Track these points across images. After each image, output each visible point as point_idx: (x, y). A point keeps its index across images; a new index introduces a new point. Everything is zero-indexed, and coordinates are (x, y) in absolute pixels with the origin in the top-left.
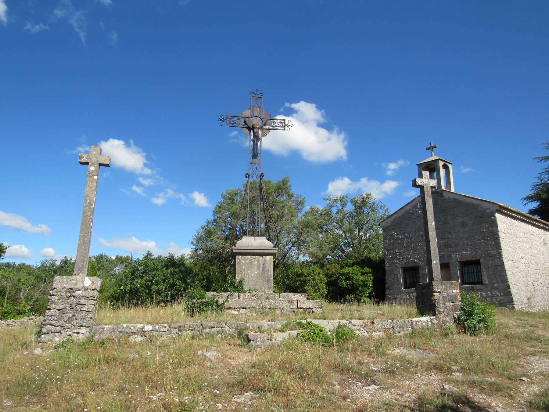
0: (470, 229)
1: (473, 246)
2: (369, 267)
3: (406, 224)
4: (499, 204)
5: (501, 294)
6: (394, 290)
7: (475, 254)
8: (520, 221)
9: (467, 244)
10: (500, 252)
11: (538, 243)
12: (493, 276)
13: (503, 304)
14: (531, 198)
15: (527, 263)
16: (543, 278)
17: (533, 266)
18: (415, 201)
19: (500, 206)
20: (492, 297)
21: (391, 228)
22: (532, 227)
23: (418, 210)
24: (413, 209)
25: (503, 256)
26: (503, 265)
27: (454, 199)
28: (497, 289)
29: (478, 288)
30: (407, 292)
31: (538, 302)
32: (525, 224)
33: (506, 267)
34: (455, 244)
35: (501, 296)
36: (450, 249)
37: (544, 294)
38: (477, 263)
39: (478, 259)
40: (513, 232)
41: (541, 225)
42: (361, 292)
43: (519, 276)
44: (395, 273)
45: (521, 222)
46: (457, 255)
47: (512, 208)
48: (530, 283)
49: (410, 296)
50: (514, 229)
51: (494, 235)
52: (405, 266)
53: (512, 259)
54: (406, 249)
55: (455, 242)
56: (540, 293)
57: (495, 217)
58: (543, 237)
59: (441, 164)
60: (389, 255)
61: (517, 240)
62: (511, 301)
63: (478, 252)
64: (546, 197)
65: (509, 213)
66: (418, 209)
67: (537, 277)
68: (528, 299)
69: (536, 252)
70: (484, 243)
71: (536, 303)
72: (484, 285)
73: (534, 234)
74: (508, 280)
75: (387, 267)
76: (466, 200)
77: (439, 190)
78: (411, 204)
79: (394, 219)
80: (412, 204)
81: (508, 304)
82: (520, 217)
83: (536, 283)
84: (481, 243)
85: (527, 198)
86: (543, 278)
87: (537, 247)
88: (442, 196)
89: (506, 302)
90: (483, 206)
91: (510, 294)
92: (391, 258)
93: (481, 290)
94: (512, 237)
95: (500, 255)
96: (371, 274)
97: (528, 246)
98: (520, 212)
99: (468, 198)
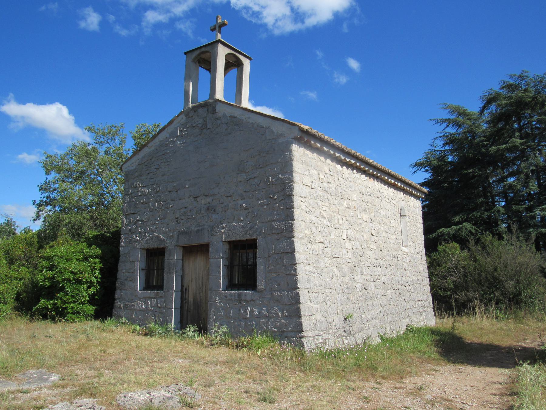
0: (249, 177)
1: (250, 210)
2: (94, 245)
3: (157, 167)
4: (302, 126)
5: (283, 313)
6: (127, 291)
7: (251, 228)
8: (355, 171)
9: (241, 206)
10: (292, 224)
11: (390, 213)
12: (275, 275)
13: (285, 334)
14: (420, 165)
15: (360, 248)
16: (390, 273)
17: (370, 253)
18: (175, 123)
19: (302, 130)
20: (268, 317)
21: (137, 174)
22: (382, 185)
23: (176, 140)
24: (170, 138)
25: (296, 234)
26: (292, 252)
27: (231, 117)
28: (278, 301)
29: (248, 298)
30: (144, 297)
31: (368, 320)
32: (368, 178)
33: (300, 256)
34: (223, 205)
35: (283, 317)
36: (214, 216)
37: (386, 303)
38: (252, 245)
39: (255, 237)
40: (333, 189)
41: (399, 184)
42: (67, 294)
43: (331, 273)
44: (131, 259)
45: (357, 172)
46: (223, 228)
47: (375, 163)
48: (359, 286)
49: (147, 304)
50: (338, 182)
51: (285, 188)
52: (147, 246)
53: (319, 238)
54: (151, 213)
55: (223, 203)
56: (377, 302)
57: (290, 152)
58: (402, 204)
59: (222, 52)
60: (128, 225)
61: (342, 205)
62: (299, 329)
63: (256, 224)
64: (437, 164)
65: (348, 160)
66: (177, 137)
67: (376, 273)
68: (346, 319)
69: (382, 228)
70: (267, 205)
71: (365, 322)
72: (258, 292)
73: (383, 197)
74: (299, 286)
75: (123, 247)
76: (249, 118)
77: (211, 101)
78: (169, 128)
79: (143, 157)
80: (169, 129)
81: (292, 334)
82: (386, 178)
83: (372, 284)
84: (262, 205)
85: (416, 165)
86: (390, 273)
87: (386, 221)
88: (214, 112)
89: (292, 331)
90: (274, 129)
91: (297, 314)
92: (130, 230)
93: (252, 302)
94: (330, 197)
95: (290, 230)
96: (97, 260)
97: (365, 217)
98: (387, 169)
99: (253, 114)
